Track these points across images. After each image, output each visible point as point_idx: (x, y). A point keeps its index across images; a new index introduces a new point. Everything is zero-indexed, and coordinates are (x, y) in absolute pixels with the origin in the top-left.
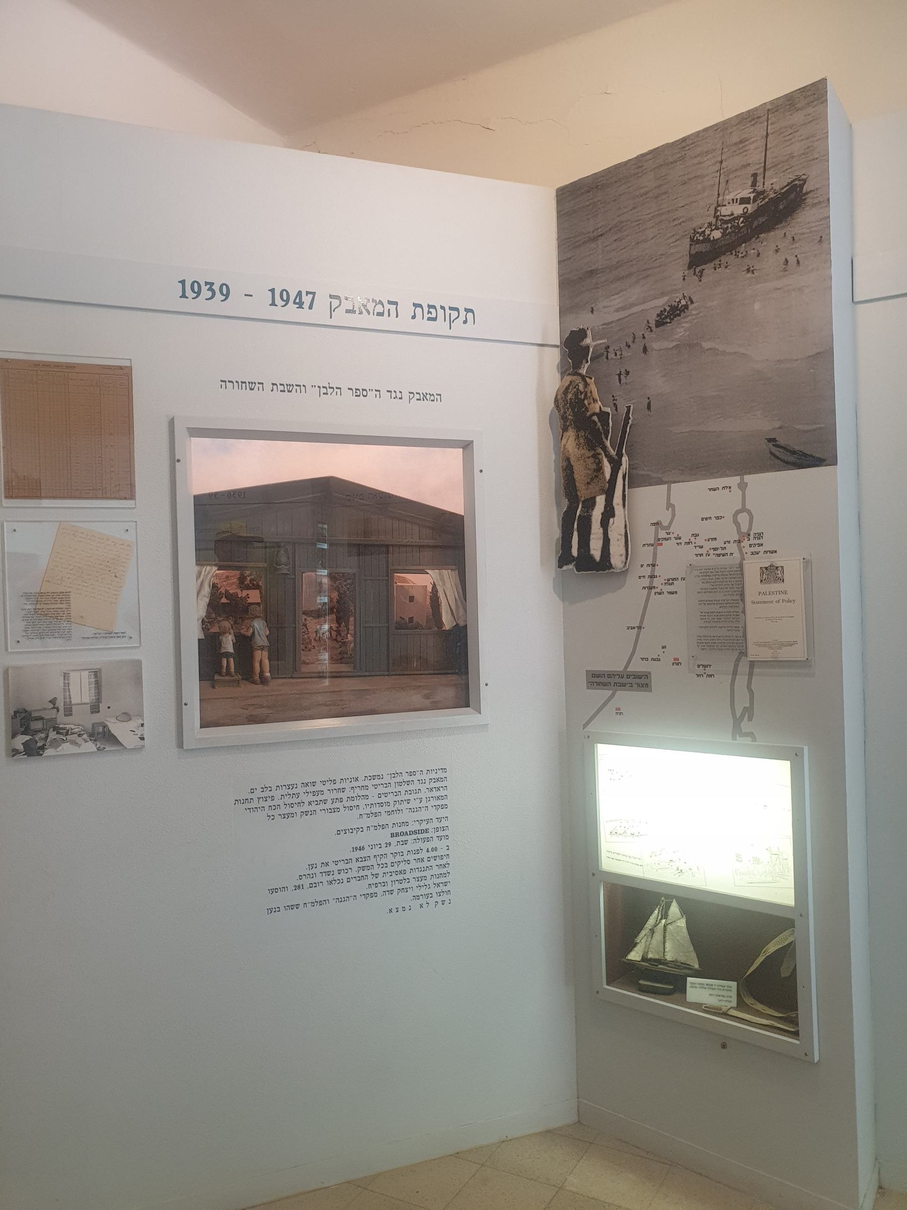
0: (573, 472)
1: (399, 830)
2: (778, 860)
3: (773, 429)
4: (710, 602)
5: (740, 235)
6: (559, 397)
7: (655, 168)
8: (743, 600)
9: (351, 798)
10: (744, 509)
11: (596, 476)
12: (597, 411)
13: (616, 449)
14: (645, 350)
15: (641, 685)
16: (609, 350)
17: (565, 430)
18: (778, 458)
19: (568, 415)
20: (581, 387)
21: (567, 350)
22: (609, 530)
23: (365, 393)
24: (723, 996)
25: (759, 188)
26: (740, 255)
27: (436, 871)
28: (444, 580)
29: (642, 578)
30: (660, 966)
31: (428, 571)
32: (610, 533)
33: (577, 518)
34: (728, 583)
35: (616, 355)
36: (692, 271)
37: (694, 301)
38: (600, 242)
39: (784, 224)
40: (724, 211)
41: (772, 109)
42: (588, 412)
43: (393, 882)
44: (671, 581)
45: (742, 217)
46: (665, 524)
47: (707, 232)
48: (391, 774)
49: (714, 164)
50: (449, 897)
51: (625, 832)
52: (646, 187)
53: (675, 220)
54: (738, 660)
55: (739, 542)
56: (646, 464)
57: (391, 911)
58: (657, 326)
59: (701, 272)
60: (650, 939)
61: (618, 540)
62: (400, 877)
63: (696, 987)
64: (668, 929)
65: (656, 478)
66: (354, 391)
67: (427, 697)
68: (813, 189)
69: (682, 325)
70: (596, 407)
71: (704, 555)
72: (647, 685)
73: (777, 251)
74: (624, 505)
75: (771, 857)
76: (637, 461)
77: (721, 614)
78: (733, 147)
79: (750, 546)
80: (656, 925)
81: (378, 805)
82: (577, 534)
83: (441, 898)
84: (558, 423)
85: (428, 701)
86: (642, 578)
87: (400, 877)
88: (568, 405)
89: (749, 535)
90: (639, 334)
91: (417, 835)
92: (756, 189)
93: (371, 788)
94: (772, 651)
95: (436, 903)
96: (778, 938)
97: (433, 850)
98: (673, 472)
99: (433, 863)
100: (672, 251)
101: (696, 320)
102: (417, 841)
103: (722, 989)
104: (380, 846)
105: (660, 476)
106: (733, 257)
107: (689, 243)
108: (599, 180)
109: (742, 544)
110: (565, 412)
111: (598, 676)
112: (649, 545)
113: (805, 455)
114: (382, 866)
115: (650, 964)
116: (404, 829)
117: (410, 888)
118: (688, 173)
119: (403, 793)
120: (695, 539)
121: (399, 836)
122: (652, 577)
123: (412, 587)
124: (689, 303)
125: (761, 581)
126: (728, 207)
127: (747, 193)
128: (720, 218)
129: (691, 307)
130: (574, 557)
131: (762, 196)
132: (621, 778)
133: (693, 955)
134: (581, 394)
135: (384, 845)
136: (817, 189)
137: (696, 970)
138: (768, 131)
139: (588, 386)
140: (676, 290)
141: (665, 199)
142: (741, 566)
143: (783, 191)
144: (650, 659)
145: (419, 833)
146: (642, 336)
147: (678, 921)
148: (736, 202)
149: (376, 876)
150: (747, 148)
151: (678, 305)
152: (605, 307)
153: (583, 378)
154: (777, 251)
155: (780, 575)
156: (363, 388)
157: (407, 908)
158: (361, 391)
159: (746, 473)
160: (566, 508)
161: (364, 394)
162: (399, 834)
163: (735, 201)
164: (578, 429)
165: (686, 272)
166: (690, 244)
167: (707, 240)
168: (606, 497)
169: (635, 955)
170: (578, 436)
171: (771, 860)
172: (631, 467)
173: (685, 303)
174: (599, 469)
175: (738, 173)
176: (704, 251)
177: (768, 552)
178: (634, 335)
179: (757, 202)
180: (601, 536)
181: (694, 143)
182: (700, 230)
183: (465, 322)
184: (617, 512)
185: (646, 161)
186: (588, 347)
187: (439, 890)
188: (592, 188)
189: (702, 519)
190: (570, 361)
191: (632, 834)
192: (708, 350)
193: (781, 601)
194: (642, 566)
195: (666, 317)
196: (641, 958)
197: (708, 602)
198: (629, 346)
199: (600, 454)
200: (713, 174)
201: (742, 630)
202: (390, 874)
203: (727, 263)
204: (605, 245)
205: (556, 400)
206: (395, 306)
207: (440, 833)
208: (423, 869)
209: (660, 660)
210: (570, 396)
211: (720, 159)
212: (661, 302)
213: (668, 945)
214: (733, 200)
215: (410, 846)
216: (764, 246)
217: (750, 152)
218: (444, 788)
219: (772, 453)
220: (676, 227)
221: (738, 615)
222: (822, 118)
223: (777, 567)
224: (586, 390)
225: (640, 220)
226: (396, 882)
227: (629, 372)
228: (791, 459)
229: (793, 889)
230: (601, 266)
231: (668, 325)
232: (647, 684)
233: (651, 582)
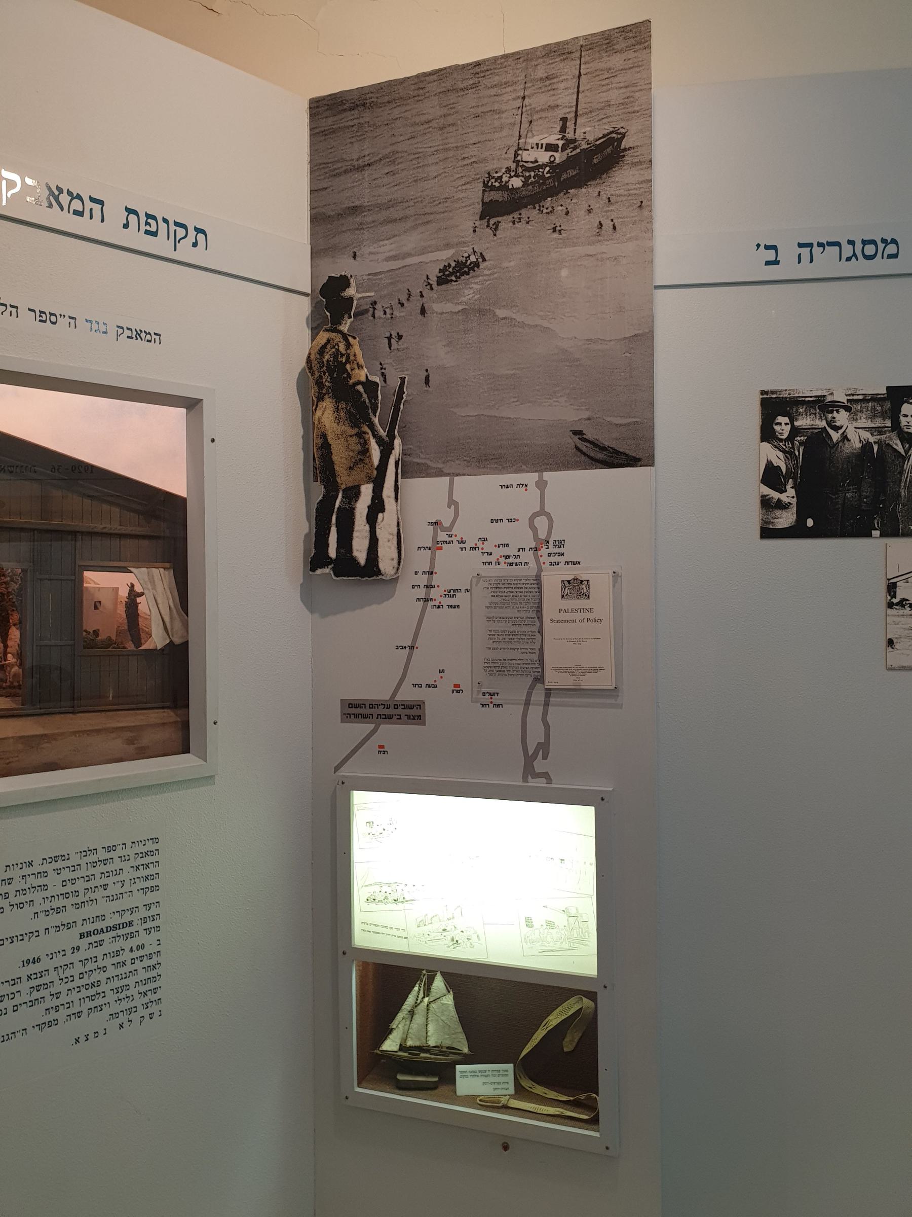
0: (332, 453)
1: (90, 927)
2: (577, 923)
3: (580, 420)
4: (501, 620)
5: (545, 187)
6: (312, 357)
7: (440, 93)
8: (540, 618)
9: (21, 891)
10: (542, 512)
11: (361, 460)
12: (363, 379)
13: (387, 429)
14: (423, 311)
15: (412, 717)
16: (376, 307)
17: (320, 398)
18: (585, 454)
19: (324, 380)
20: (342, 347)
21: (324, 300)
22: (377, 527)
23: (53, 319)
24: (499, 1083)
25: (570, 135)
26: (545, 211)
27: (143, 975)
28: (154, 581)
29: (416, 587)
30: (422, 1055)
31: (132, 569)
32: (378, 531)
33: (336, 510)
34: (523, 597)
35: (385, 313)
36: (485, 222)
37: (487, 259)
38: (367, 172)
39: (598, 181)
40: (527, 156)
41: (586, 45)
42: (350, 379)
43: (82, 1000)
44: (452, 593)
45: (548, 166)
46: (446, 524)
47: (505, 179)
48: (81, 852)
49: (514, 99)
50: (159, 1007)
51: (386, 898)
52: (428, 113)
53: (464, 158)
54: (532, 688)
55: (536, 550)
56: (423, 451)
57: (77, 1041)
58: (439, 284)
59: (497, 225)
60: (408, 1023)
61: (389, 541)
62: (92, 991)
63: (467, 1077)
64: (431, 1009)
65: (435, 468)
66: (38, 314)
67: (131, 741)
68: (632, 146)
69: (471, 286)
70: (361, 375)
71: (494, 563)
72: (419, 717)
73: (589, 211)
74: (396, 499)
75: (568, 920)
76: (411, 446)
77: (513, 633)
78: (538, 83)
79: (549, 555)
80: (416, 1005)
81: (61, 897)
82: (336, 531)
83: (149, 1011)
84: (313, 392)
85: (132, 746)
86: (416, 587)
87: (92, 991)
88: (325, 368)
89: (548, 542)
90: (415, 292)
91: (117, 931)
92: (565, 136)
93: (51, 873)
94: (575, 678)
95: (142, 1019)
96: (560, 1008)
97: (138, 948)
98: (457, 462)
99: (138, 965)
100: (461, 195)
101: (489, 282)
102: (117, 939)
103: (497, 1074)
104: (63, 953)
105: (440, 466)
106: (536, 212)
107: (482, 189)
108: (368, 96)
109: (540, 553)
110: (320, 377)
111: (357, 706)
112: (425, 548)
113: (617, 452)
114: (66, 980)
115: (410, 1054)
116: (99, 925)
117: (105, 1004)
118: (483, 105)
119: (98, 876)
120: (483, 544)
121: (91, 936)
122: (429, 587)
123: (99, 589)
124: (480, 260)
125: (563, 596)
126: (531, 152)
127: (554, 138)
128: (521, 163)
129: (482, 265)
130: (331, 558)
131: (572, 146)
132: (382, 831)
133: (462, 1037)
134: (341, 357)
135: (69, 952)
136: (637, 146)
137: (465, 1055)
138: (581, 71)
139: (351, 347)
140: (464, 243)
141: (452, 132)
142: (538, 579)
143: (598, 143)
144: (424, 686)
145: (119, 929)
146: (420, 294)
147: (444, 998)
148: (542, 148)
149: (57, 995)
150: (555, 86)
151: (466, 261)
152: (371, 253)
153: (345, 336)
154: (589, 211)
155: (585, 591)
156: (52, 312)
157: (101, 1032)
158: (48, 316)
159: (546, 470)
160: (322, 496)
161: (52, 320)
162: (92, 933)
163: (540, 146)
164: (337, 399)
165: (478, 223)
166: (483, 190)
167: (504, 187)
168: (374, 487)
169: (390, 1045)
170: (338, 408)
171: (568, 924)
172: (404, 453)
173: (476, 260)
174: (365, 451)
175: (544, 114)
176: (500, 200)
177: (570, 563)
178: (409, 291)
179: (567, 152)
180: (367, 534)
181: (491, 70)
182: (496, 175)
183: (195, 245)
184: (387, 506)
185: (429, 83)
186: (351, 299)
187: (146, 1000)
188: (357, 106)
189: (492, 521)
190: (328, 314)
191: (395, 900)
192: (503, 319)
193: (585, 620)
194: (416, 573)
195: (451, 274)
196: (398, 1046)
197: (498, 619)
198: (402, 305)
199: (365, 433)
200: (513, 111)
201: (537, 652)
202: (78, 990)
203: (529, 218)
204: (373, 178)
205: (309, 360)
206: (101, 206)
207: (149, 924)
208: (124, 976)
209: (436, 687)
210: (327, 357)
211: (522, 95)
212: (445, 256)
213: (431, 1028)
214: (537, 144)
215: (108, 947)
216: (574, 203)
217: (559, 92)
218: (155, 864)
219: (577, 448)
220: (466, 167)
221: (535, 636)
222: (644, 66)
223: (582, 582)
224: (348, 352)
225: (420, 153)
226: (86, 999)
227: (402, 336)
228: (600, 456)
229: (596, 956)
230: (368, 202)
231: (453, 283)
232: (420, 716)
233: (428, 593)
